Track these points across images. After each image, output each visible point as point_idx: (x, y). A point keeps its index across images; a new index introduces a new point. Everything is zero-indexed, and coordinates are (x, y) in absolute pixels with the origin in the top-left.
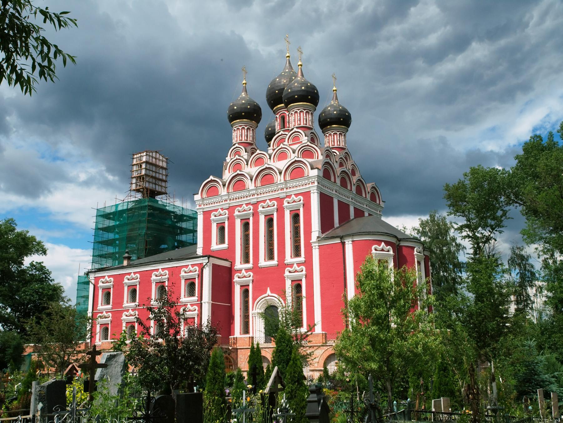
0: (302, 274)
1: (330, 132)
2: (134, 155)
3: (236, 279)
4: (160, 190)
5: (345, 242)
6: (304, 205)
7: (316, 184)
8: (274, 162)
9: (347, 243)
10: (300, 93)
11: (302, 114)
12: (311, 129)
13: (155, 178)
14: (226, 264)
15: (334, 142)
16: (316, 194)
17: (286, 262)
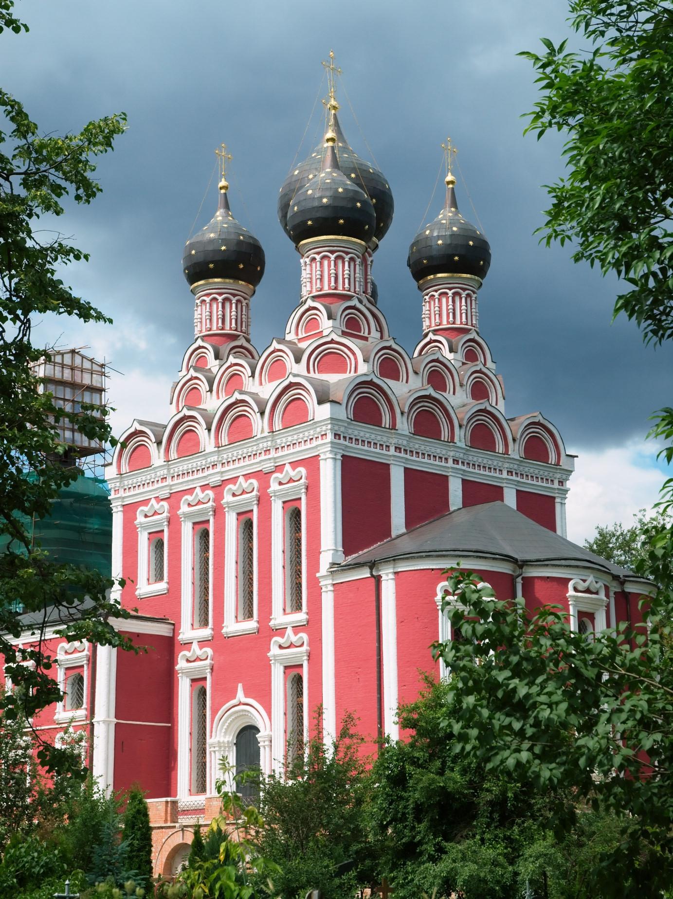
0: (300, 654)
3: (181, 664)
4: (86, 444)
5: (380, 577)
6: (307, 489)
7: (330, 437)
8: (261, 384)
9: (384, 577)
10: (319, 215)
11: (326, 262)
14: (162, 630)
15: (440, 315)
16: (330, 463)
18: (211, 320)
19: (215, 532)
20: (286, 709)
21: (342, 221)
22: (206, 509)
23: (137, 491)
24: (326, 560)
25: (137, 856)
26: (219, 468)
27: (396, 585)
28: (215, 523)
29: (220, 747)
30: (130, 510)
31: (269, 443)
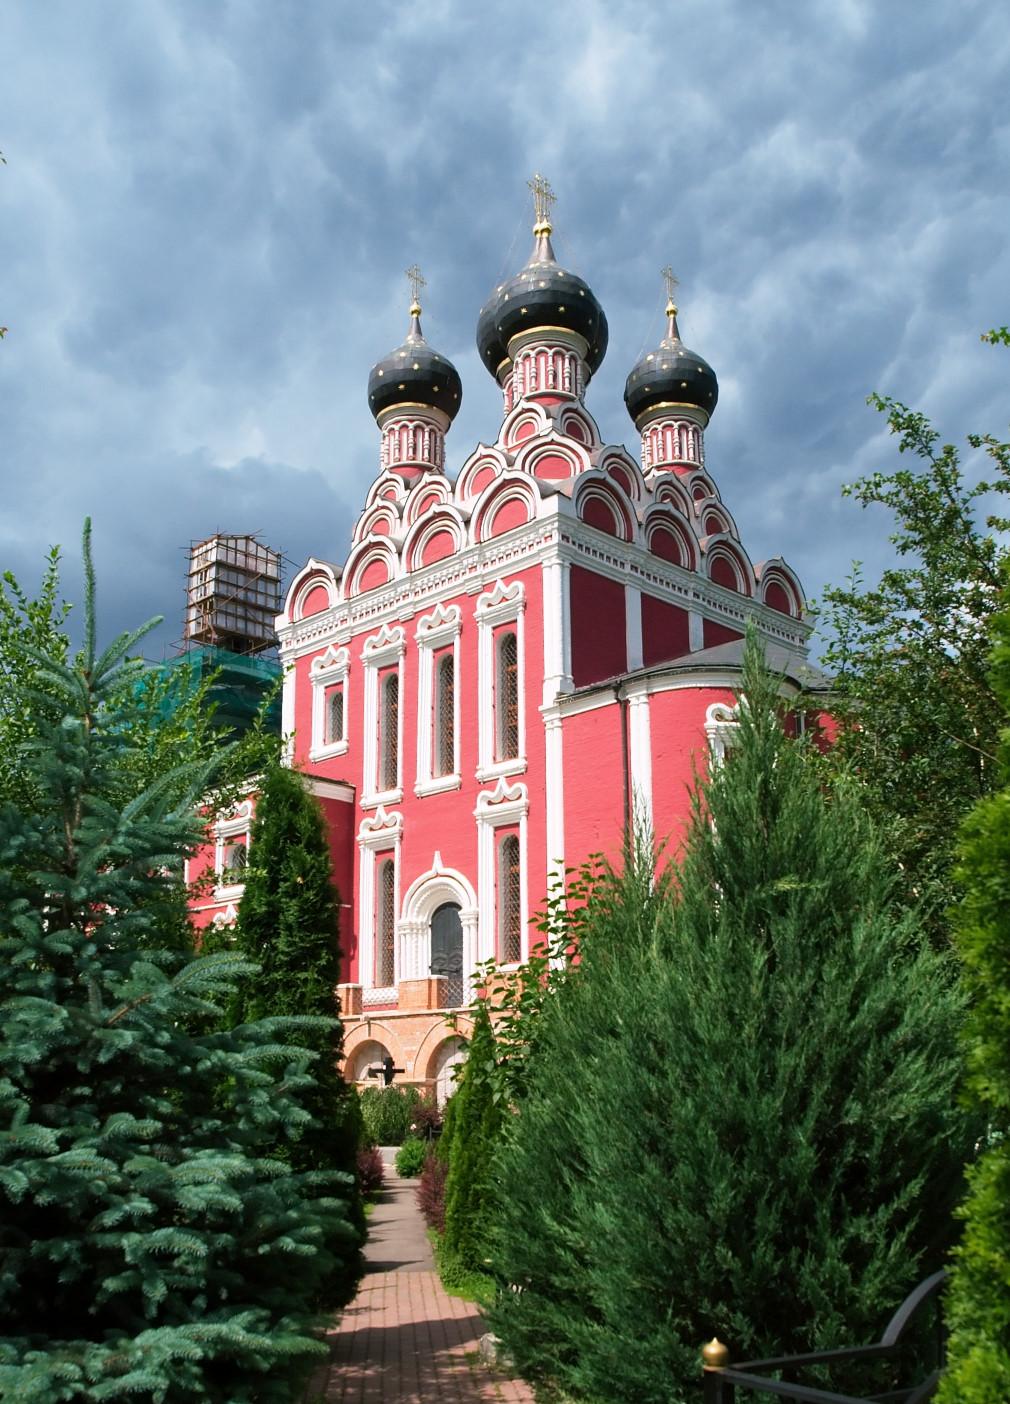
1: (653, 425)
2: (193, 550)
3: (363, 834)
5: (628, 701)
6: (525, 606)
7: (556, 538)
8: (463, 499)
9: (633, 701)
10: (535, 300)
12: (695, 468)
13: (245, 604)
14: (339, 794)
15: (664, 450)
16: (557, 570)
17: (478, 775)
18: (400, 450)
19: (406, 675)
20: (496, 879)
21: (562, 309)
22: (395, 649)
23: (313, 640)
24: (551, 688)
25: (289, 985)
26: (411, 598)
27: (651, 710)
28: (405, 664)
29: (412, 930)
30: (303, 663)
31: (476, 558)
